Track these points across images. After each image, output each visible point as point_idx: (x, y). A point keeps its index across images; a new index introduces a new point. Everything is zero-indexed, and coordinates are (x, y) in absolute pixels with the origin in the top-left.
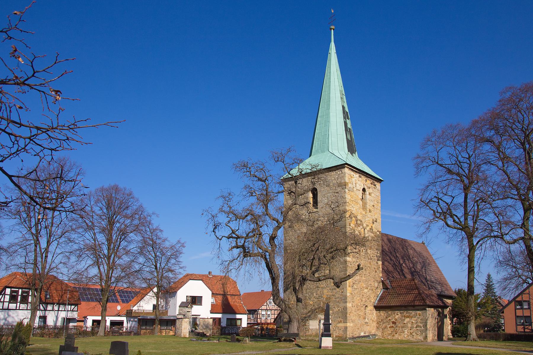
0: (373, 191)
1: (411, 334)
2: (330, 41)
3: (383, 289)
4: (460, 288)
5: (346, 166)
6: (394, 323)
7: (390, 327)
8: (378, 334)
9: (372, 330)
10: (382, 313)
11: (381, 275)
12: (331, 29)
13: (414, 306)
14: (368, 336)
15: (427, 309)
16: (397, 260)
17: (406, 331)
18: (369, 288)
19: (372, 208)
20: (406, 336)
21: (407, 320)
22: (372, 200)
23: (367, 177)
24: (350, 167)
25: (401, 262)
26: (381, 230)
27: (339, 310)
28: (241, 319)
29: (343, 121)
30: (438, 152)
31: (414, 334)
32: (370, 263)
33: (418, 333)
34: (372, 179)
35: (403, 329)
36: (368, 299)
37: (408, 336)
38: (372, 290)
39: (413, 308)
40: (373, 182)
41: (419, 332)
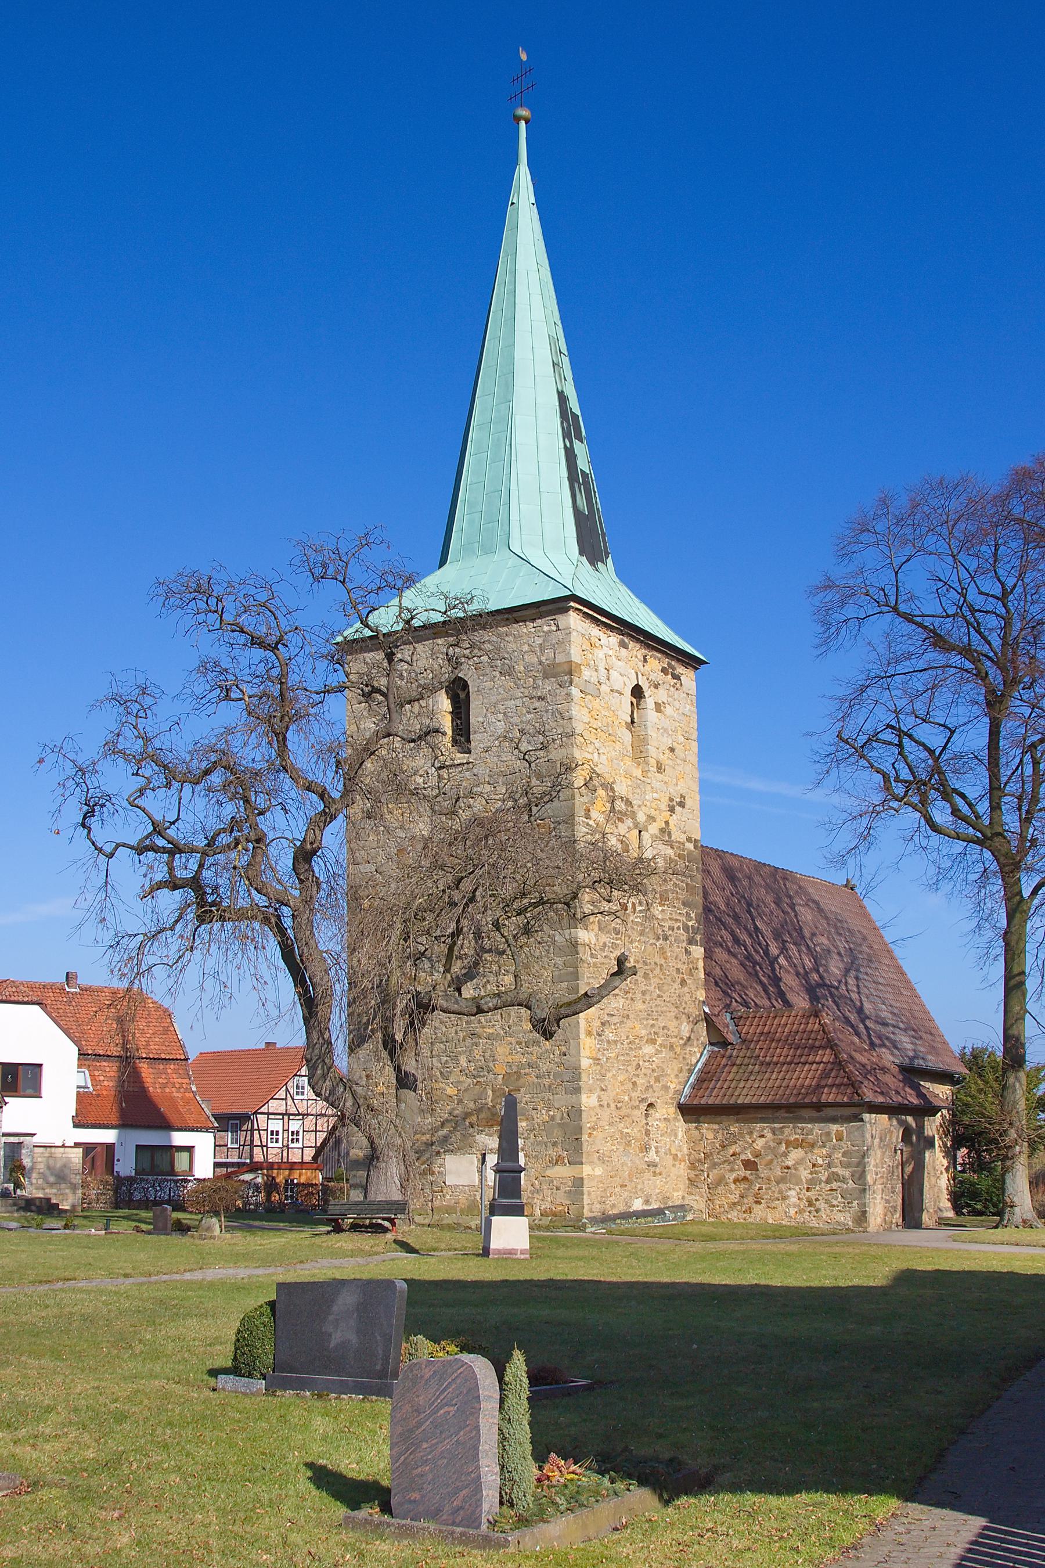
1: (810, 1205)
2: (515, 162)
3: (711, 1044)
5: (572, 604)
6: (749, 1165)
10: (707, 1129)
11: (701, 995)
12: (518, 119)
13: (819, 1107)
14: (659, 1212)
15: (866, 1116)
17: (792, 1193)
20: (792, 1211)
21: (796, 1154)
24: (586, 610)
25: (774, 950)
26: (697, 835)
27: (552, 1118)
28: (190, 1149)
30: (896, 573)
32: (662, 951)
33: (835, 1203)
37: (801, 1211)
39: (814, 1114)
40: (669, 664)
41: (840, 1199)
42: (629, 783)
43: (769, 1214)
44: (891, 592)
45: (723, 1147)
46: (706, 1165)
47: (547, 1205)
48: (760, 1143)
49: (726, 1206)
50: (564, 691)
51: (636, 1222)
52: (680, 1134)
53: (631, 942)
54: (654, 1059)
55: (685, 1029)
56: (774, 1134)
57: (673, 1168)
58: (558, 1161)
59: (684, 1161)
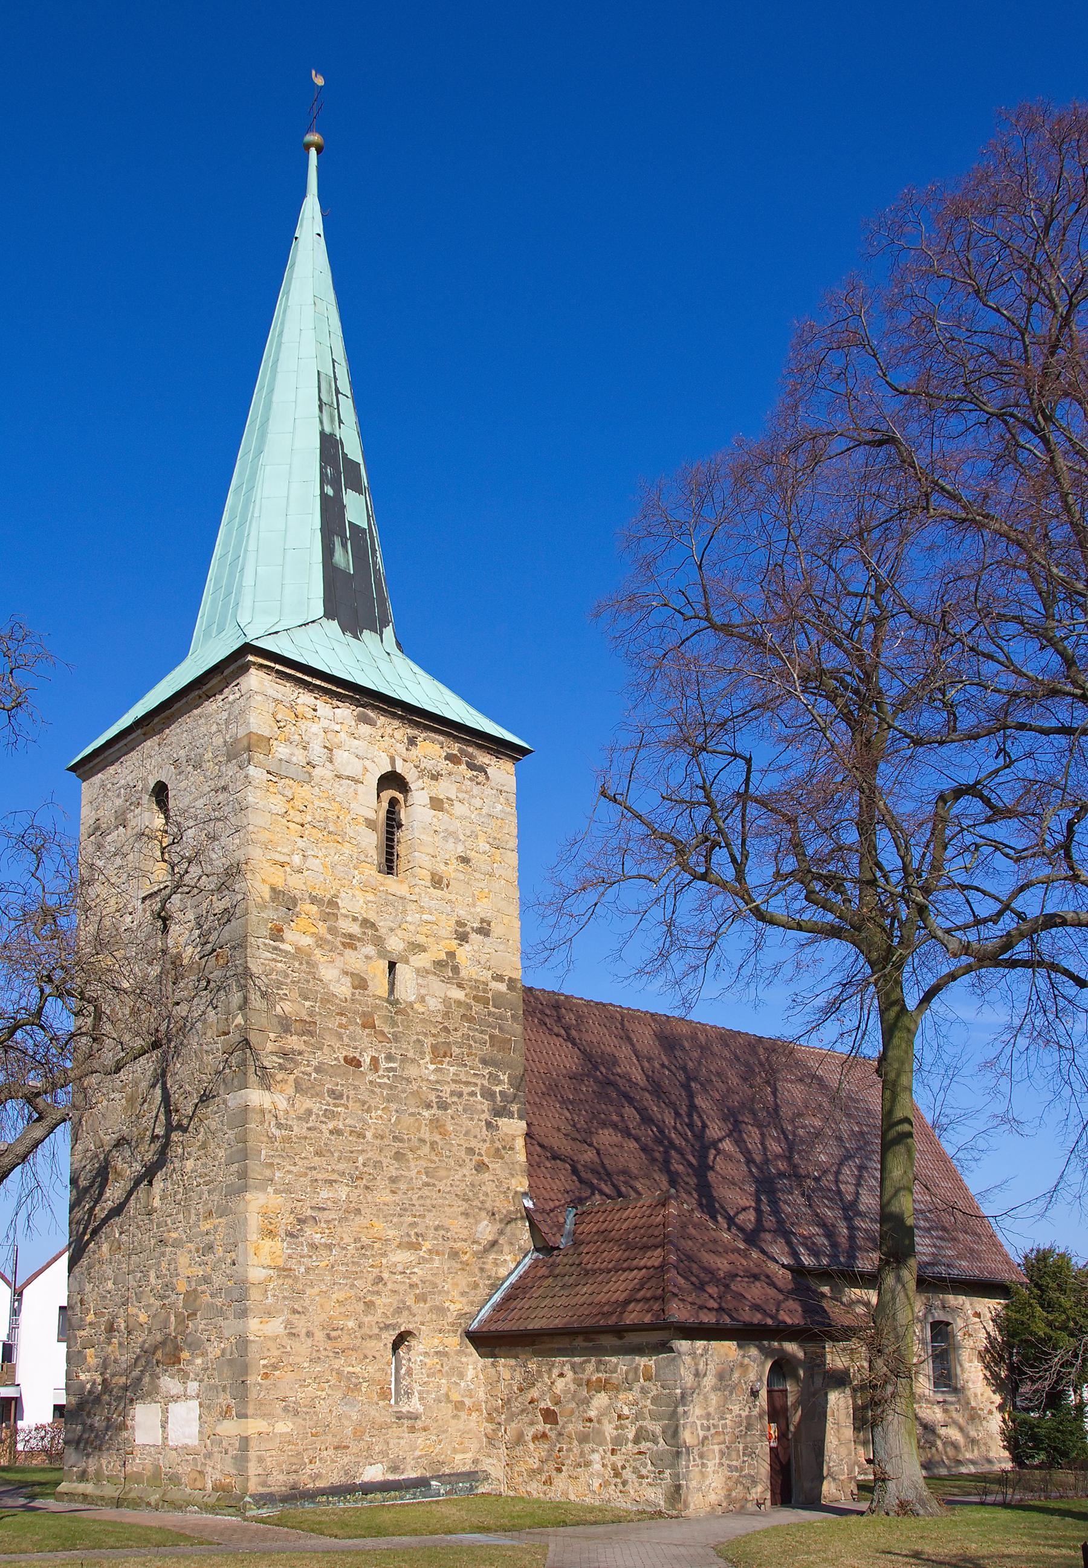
0: (459, 790)
2: (303, 194)
3: (537, 1250)
4: (1045, 1245)
5: (251, 658)
7: (535, 1438)
8: (491, 1470)
9: (455, 1451)
10: (504, 1366)
11: (521, 1184)
12: (307, 147)
14: (421, 1484)
15: (683, 1345)
16: (690, 1125)
17: (596, 1457)
18: (427, 1245)
19: (451, 871)
20: (596, 1483)
21: (601, 1400)
22: (452, 834)
23: (417, 725)
24: (278, 667)
25: (715, 1130)
26: (517, 975)
29: (318, 492)
31: (627, 1474)
32: (436, 1124)
33: (644, 1472)
34: (456, 739)
35: (587, 1447)
36: (421, 1298)
37: (605, 1484)
38: (454, 1254)
40: (460, 750)
41: (650, 1467)
42: (371, 897)
43: (571, 1488)
44: (695, 595)
45: (521, 1390)
46: (503, 1416)
47: (217, 1476)
48: (560, 1384)
49: (525, 1474)
50: (243, 773)
51: (363, 1499)
52: (470, 1373)
53: (368, 1111)
54: (416, 1270)
55: (486, 1230)
56: (575, 1373)
57: (454, 1422)
58: (226, 1414)
59: (479, 1410)
